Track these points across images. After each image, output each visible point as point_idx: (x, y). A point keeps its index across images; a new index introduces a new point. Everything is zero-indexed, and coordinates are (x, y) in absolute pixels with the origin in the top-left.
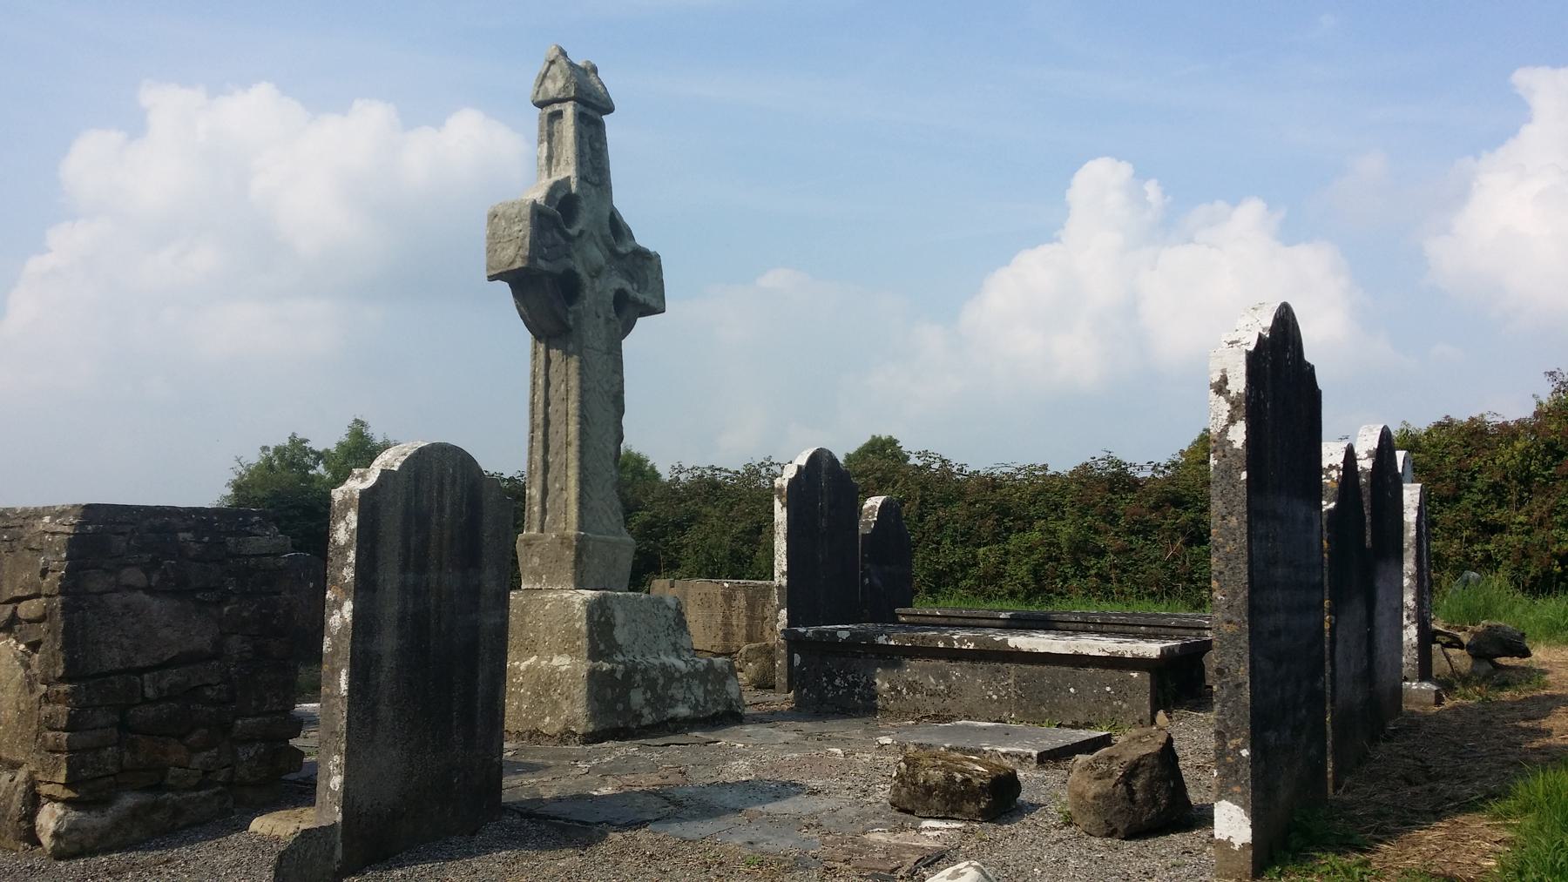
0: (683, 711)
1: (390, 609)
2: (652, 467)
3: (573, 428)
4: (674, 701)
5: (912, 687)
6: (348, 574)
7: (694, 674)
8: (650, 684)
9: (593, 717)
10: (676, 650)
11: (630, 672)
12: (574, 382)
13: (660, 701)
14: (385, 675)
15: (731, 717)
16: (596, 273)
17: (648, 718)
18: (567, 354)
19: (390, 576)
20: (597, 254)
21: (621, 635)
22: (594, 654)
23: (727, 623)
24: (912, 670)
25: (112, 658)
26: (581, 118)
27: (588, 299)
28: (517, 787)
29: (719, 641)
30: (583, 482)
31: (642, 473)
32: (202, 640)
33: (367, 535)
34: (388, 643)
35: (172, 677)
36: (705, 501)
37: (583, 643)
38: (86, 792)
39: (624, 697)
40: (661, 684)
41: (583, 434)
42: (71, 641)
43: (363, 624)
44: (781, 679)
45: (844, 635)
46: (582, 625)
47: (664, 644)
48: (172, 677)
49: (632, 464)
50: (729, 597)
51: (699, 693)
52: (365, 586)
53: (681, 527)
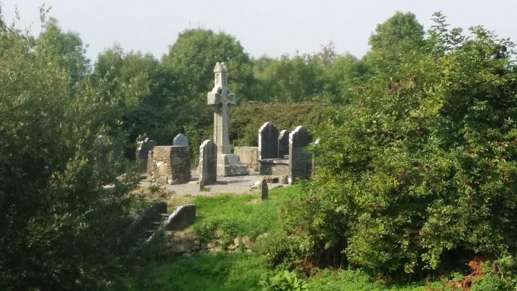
0: (239, 173)
1: (206, 158)
2: (238, 43)
3: (222, 128)
4: (237, 172)
5: (279, 170)
6: (202, 155)
7: (241, 167)
8: (234, 169)
9: (226, 173)
10: (238, 164)
11: (231, 167)
12: (222, 121)
13: (235, 171)
14: (206, 165)
15: (247, 174)
16: (224, 101)
17: (234, 174)
18: (220, 116)
19: (206, 156)
20: (225, 98)
21: (229, 161)
22: (225, 164)
23: (252, 158)
24: (279, 167)
25: (174, 164)
26: (222, 75)
27: (224, 106)
28: (218, 180)
29: (250, 162)
30: (223, 137)
31: (231, 48)
32: (181, 162)
33: (204, 151)
34: (206, 163)
35: (180, 166)
36: (253, 115)
37: (224, 162)
38: (174, 178)
39: (230, 170)
40: (236, 169)
41: (223, 129)
42: (171, 162)
43: (204, 161)
44: (259, 169)
45: (268, 161)
46: (224, 160)
47: (236, 162)
48: (180, 166)
49: (225, 42)
50: (252, 151)
51: (242, 170)
52: (204, 157)
53: (245, 124)
